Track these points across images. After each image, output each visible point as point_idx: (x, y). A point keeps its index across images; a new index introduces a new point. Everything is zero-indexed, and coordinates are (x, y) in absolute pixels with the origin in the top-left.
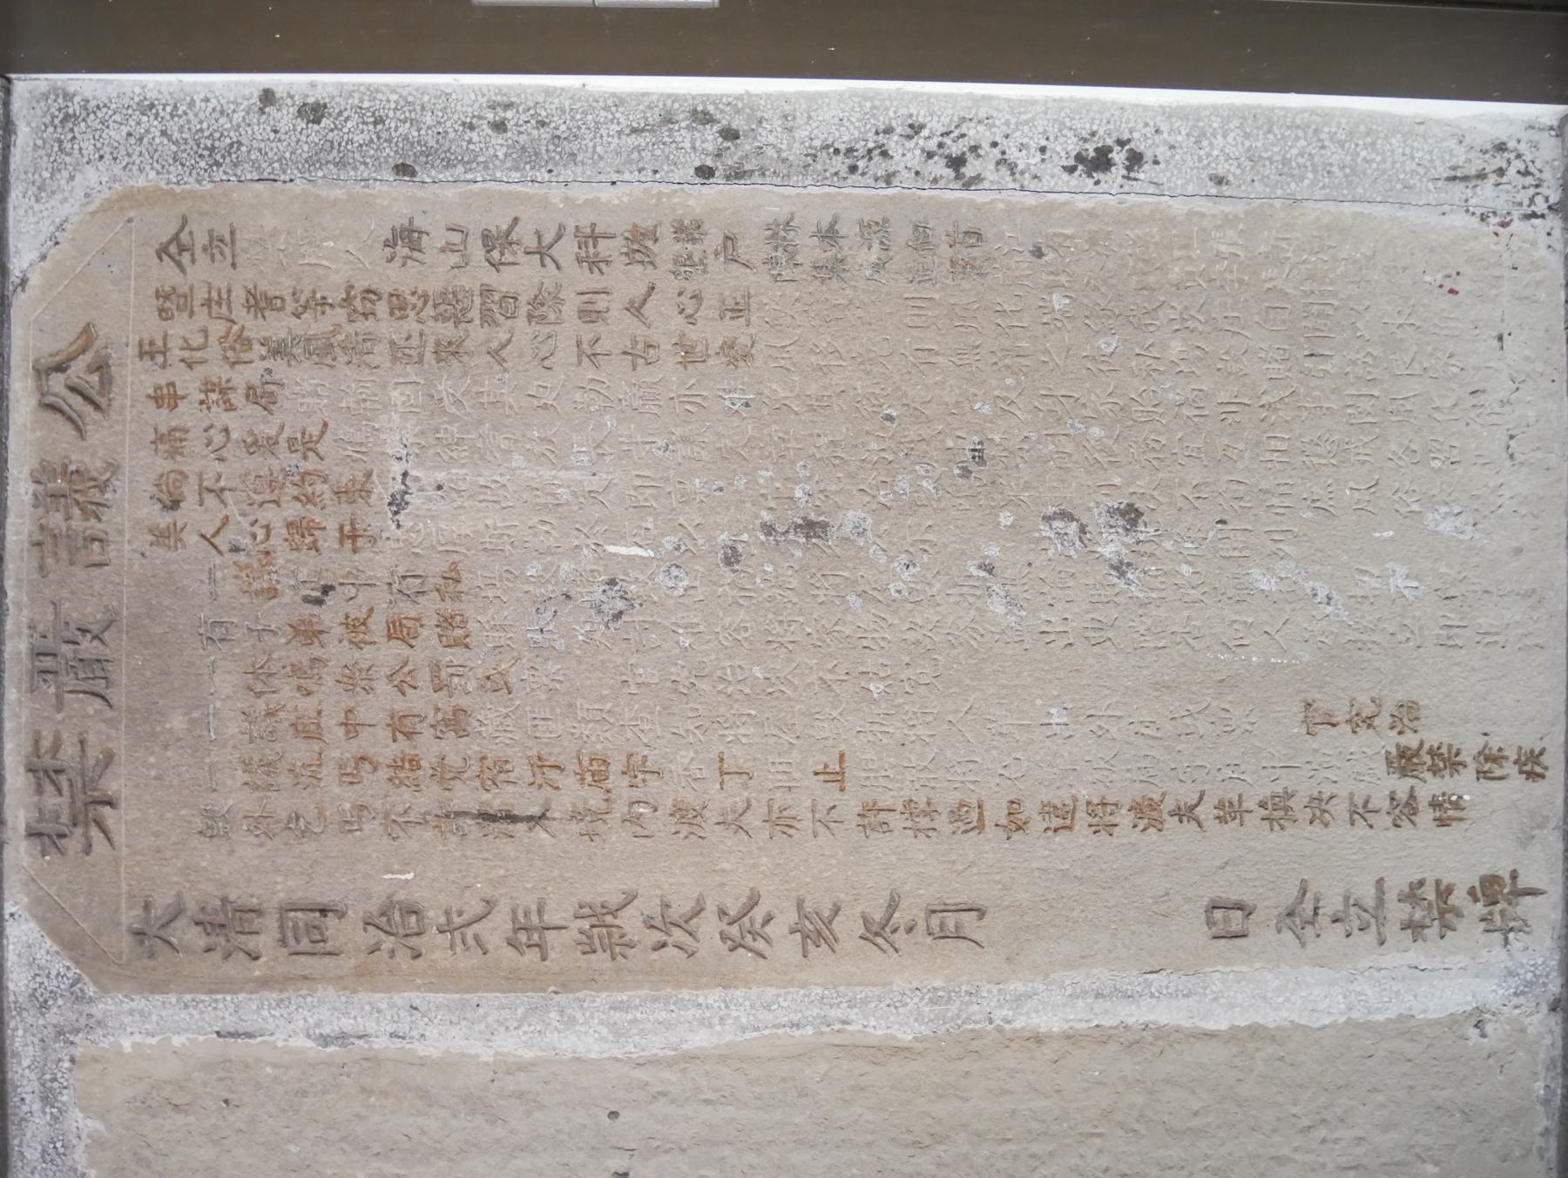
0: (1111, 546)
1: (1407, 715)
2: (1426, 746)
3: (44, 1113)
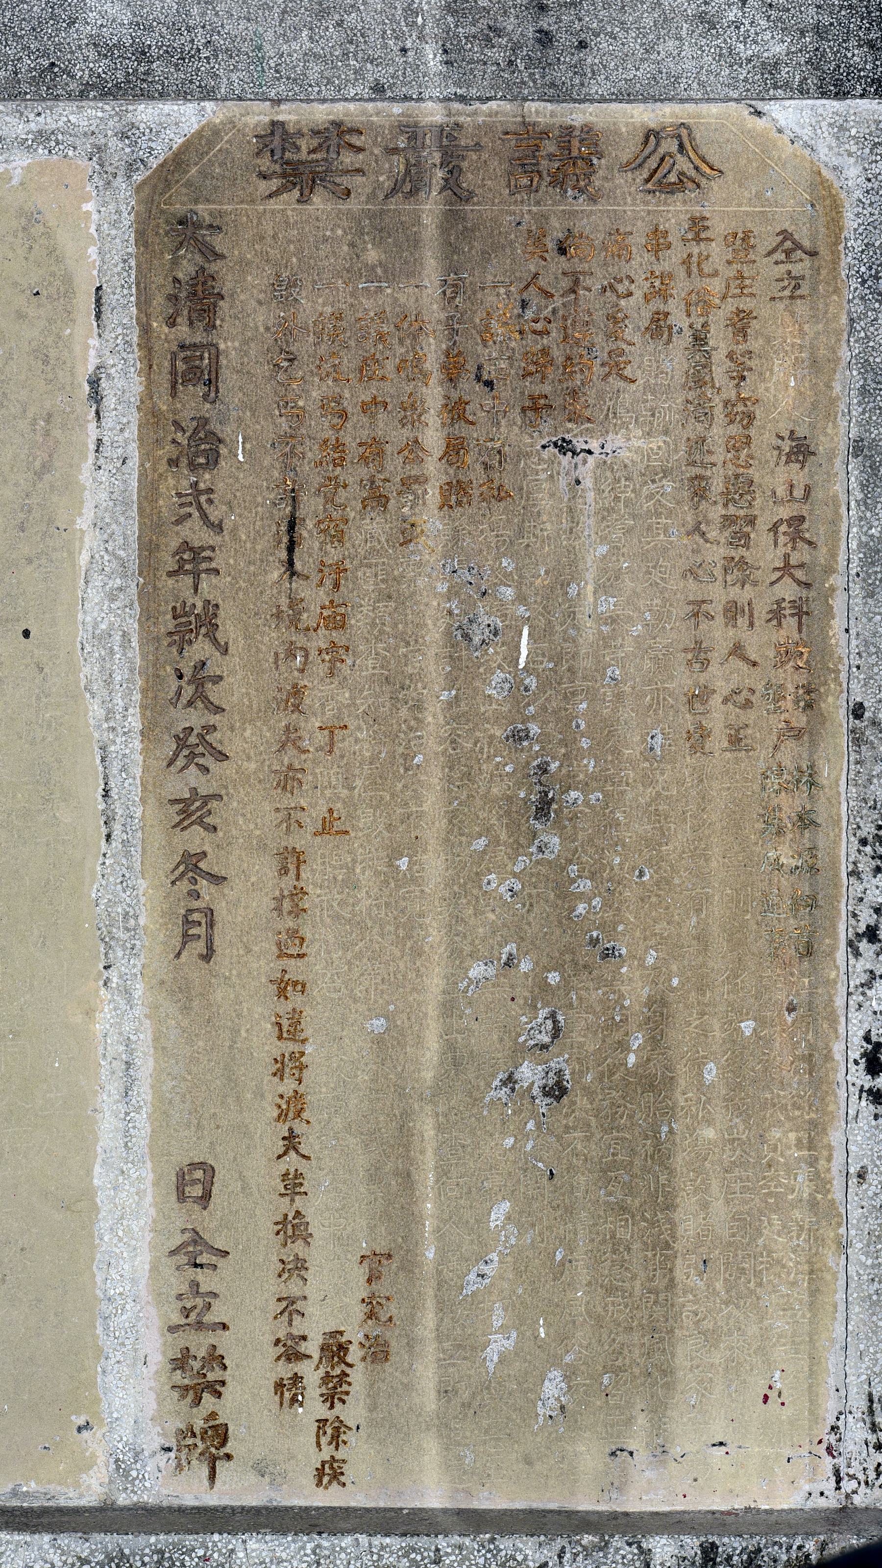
0: (529, 1073)
1: (378, 1352)
2: (348, 1370)
3: (28, 133)
